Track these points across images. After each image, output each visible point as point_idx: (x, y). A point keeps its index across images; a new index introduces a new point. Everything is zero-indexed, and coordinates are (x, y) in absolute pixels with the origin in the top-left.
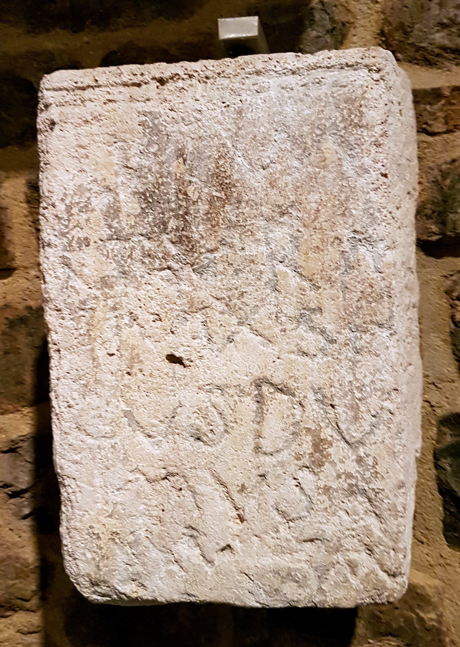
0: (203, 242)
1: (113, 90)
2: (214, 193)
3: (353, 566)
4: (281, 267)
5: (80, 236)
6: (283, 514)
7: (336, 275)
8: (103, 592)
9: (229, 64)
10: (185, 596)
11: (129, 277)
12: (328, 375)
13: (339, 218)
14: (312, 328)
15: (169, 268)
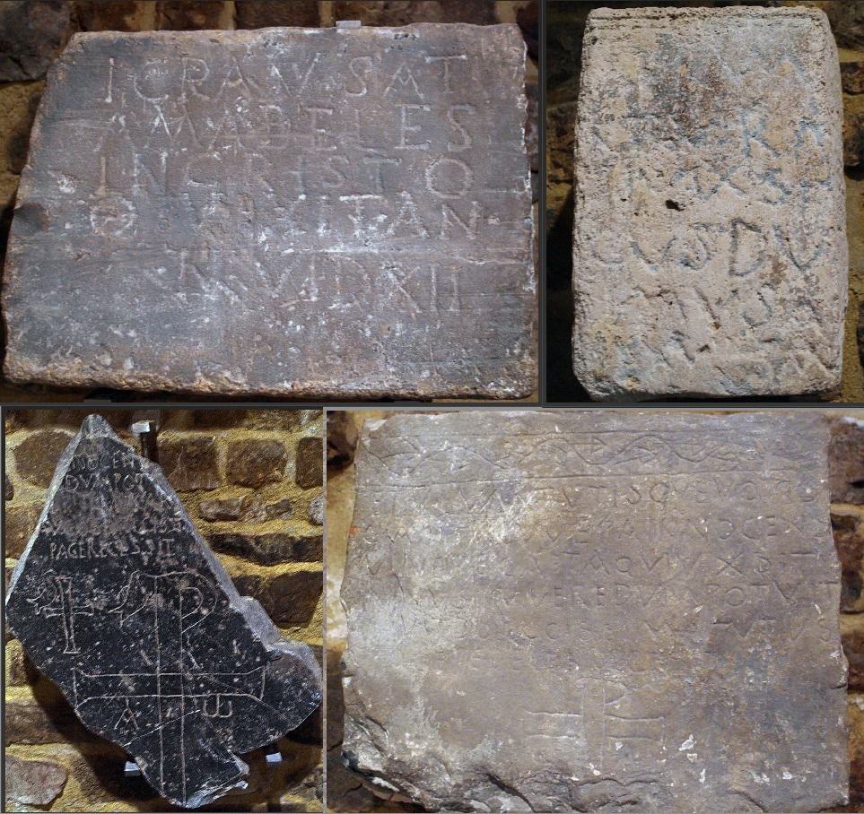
1: (641, 21)
3: (800, 360)
6: (749, 320)
15: (672, 139)
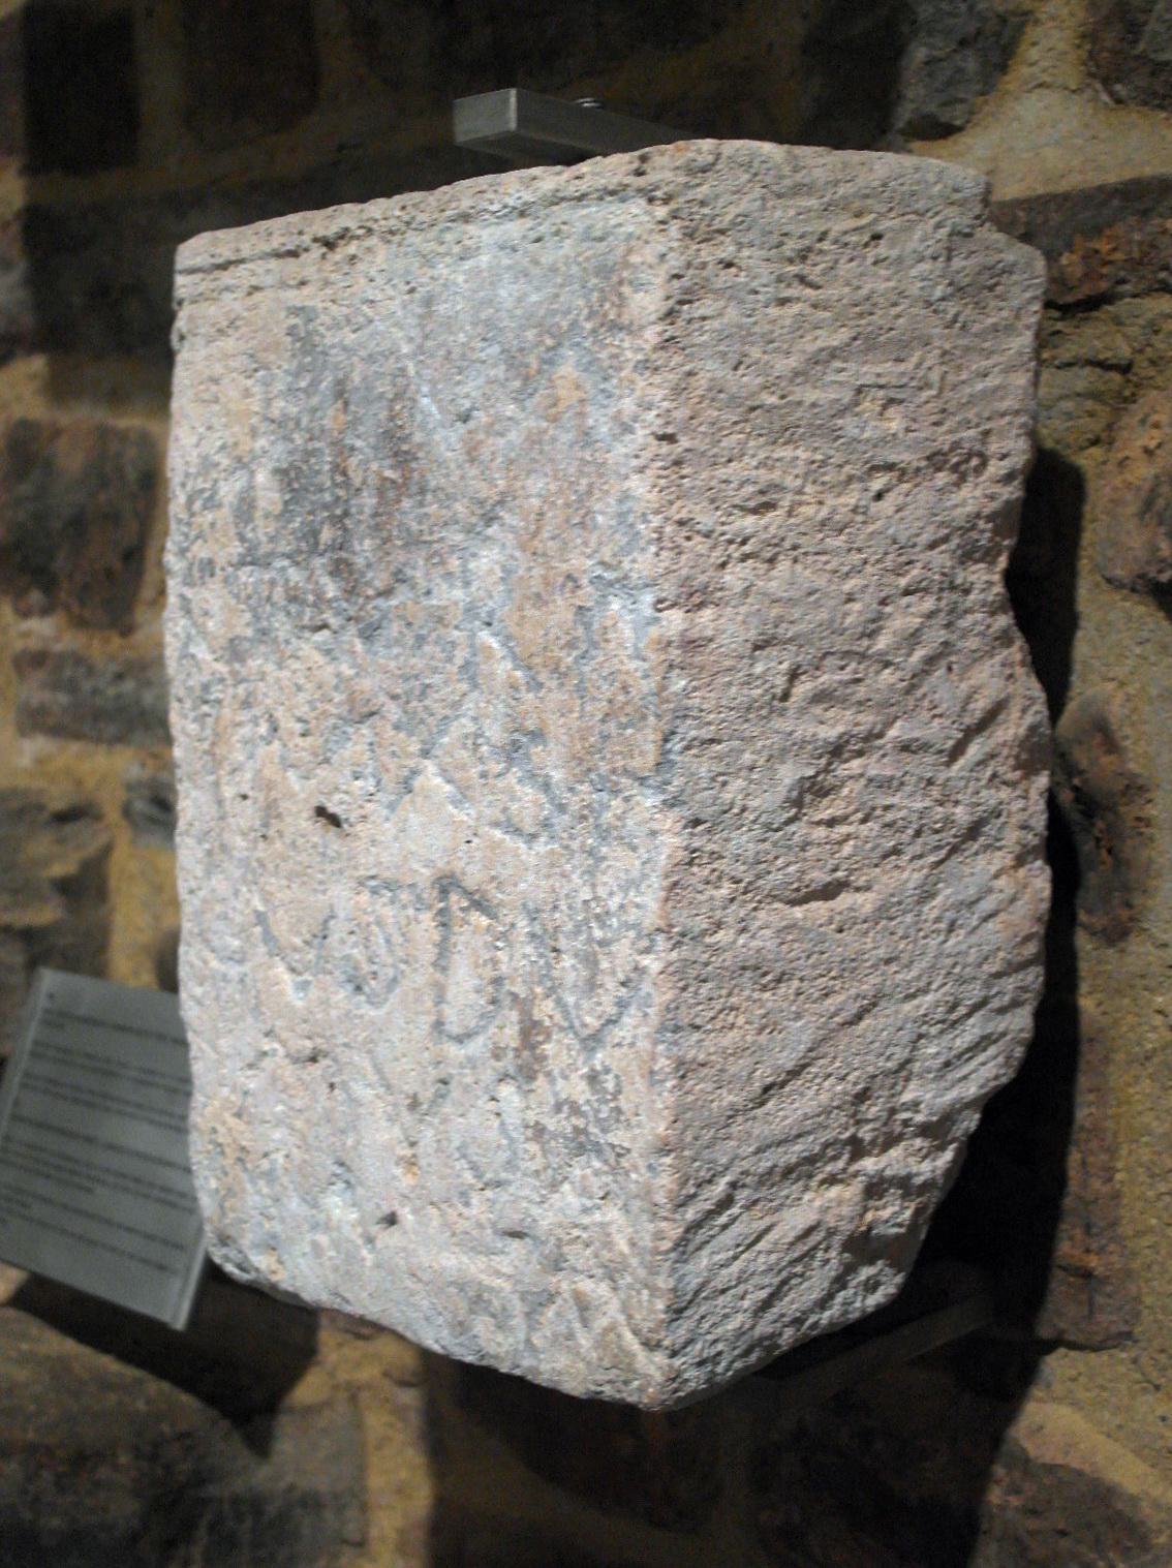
3: (583, 1305)
4: (486, 637)
12: (551, 882)
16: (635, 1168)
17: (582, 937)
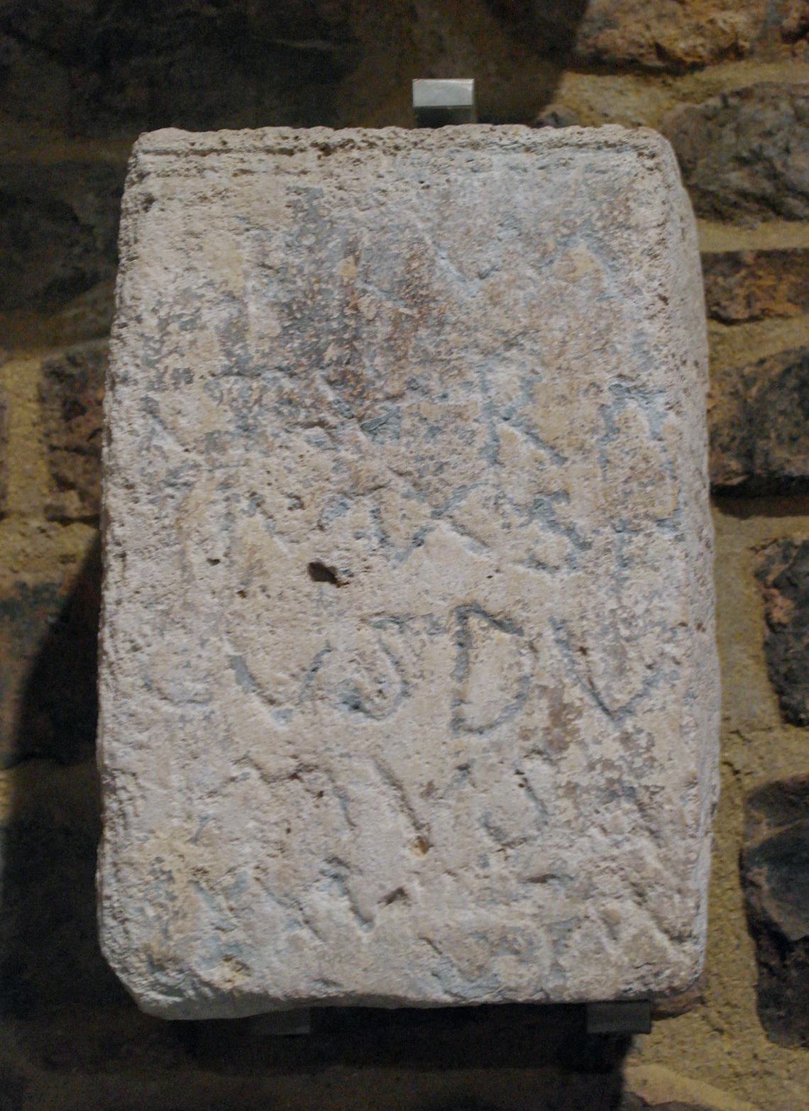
0: (379, 384)
1: (248, 156)
2: (402, 310)
3: (611, 923)
5: (178, 366)
6: (496, 833)
7: (592, 440)
8: (171, 982)
9: (432, 136)
10: (319, 985)
11: (253, 436)
12: (577, 599)
13: (596, 355)
14: (553, 525)
15: (322, 424)
16: (670, 801)
17: (611, 636)
